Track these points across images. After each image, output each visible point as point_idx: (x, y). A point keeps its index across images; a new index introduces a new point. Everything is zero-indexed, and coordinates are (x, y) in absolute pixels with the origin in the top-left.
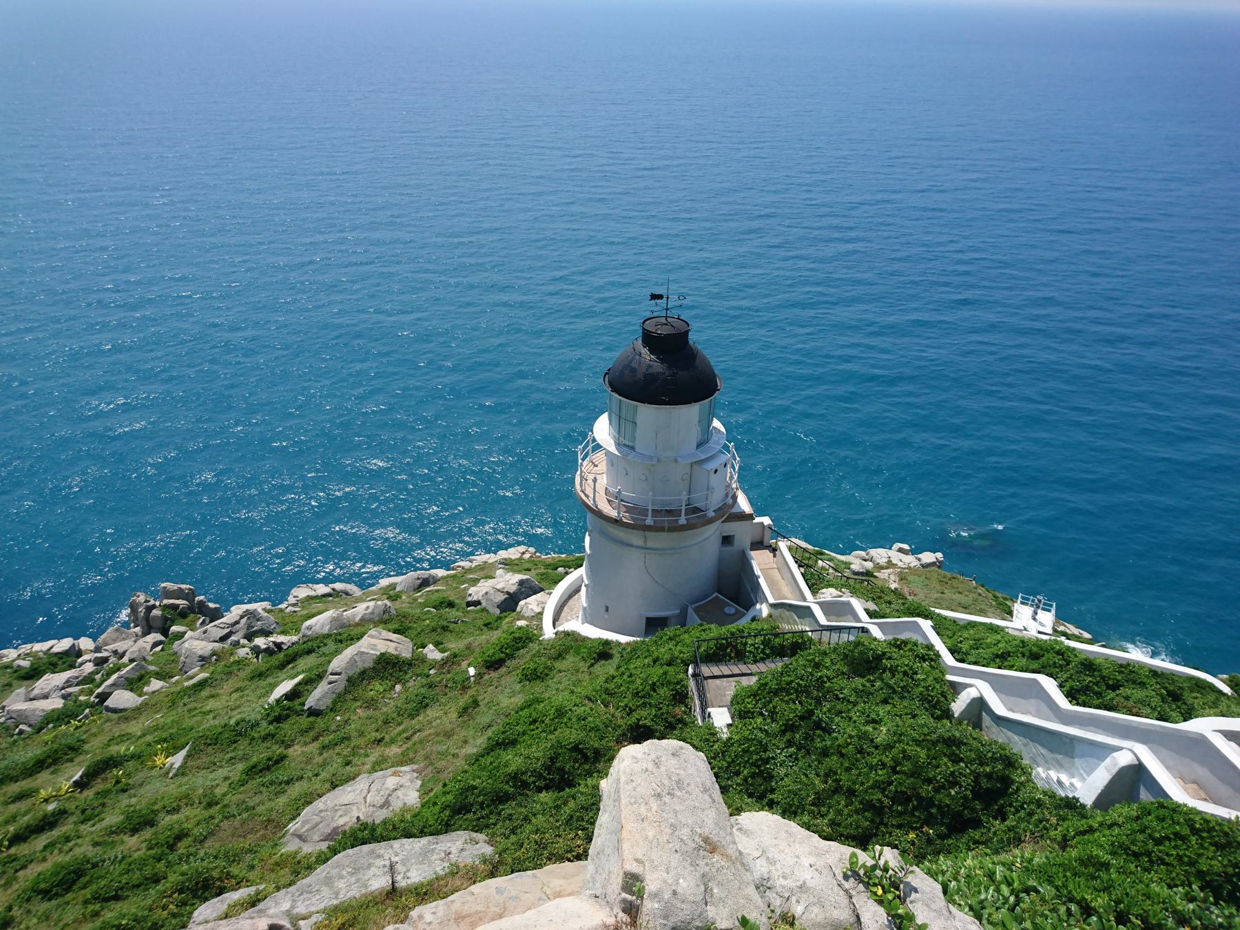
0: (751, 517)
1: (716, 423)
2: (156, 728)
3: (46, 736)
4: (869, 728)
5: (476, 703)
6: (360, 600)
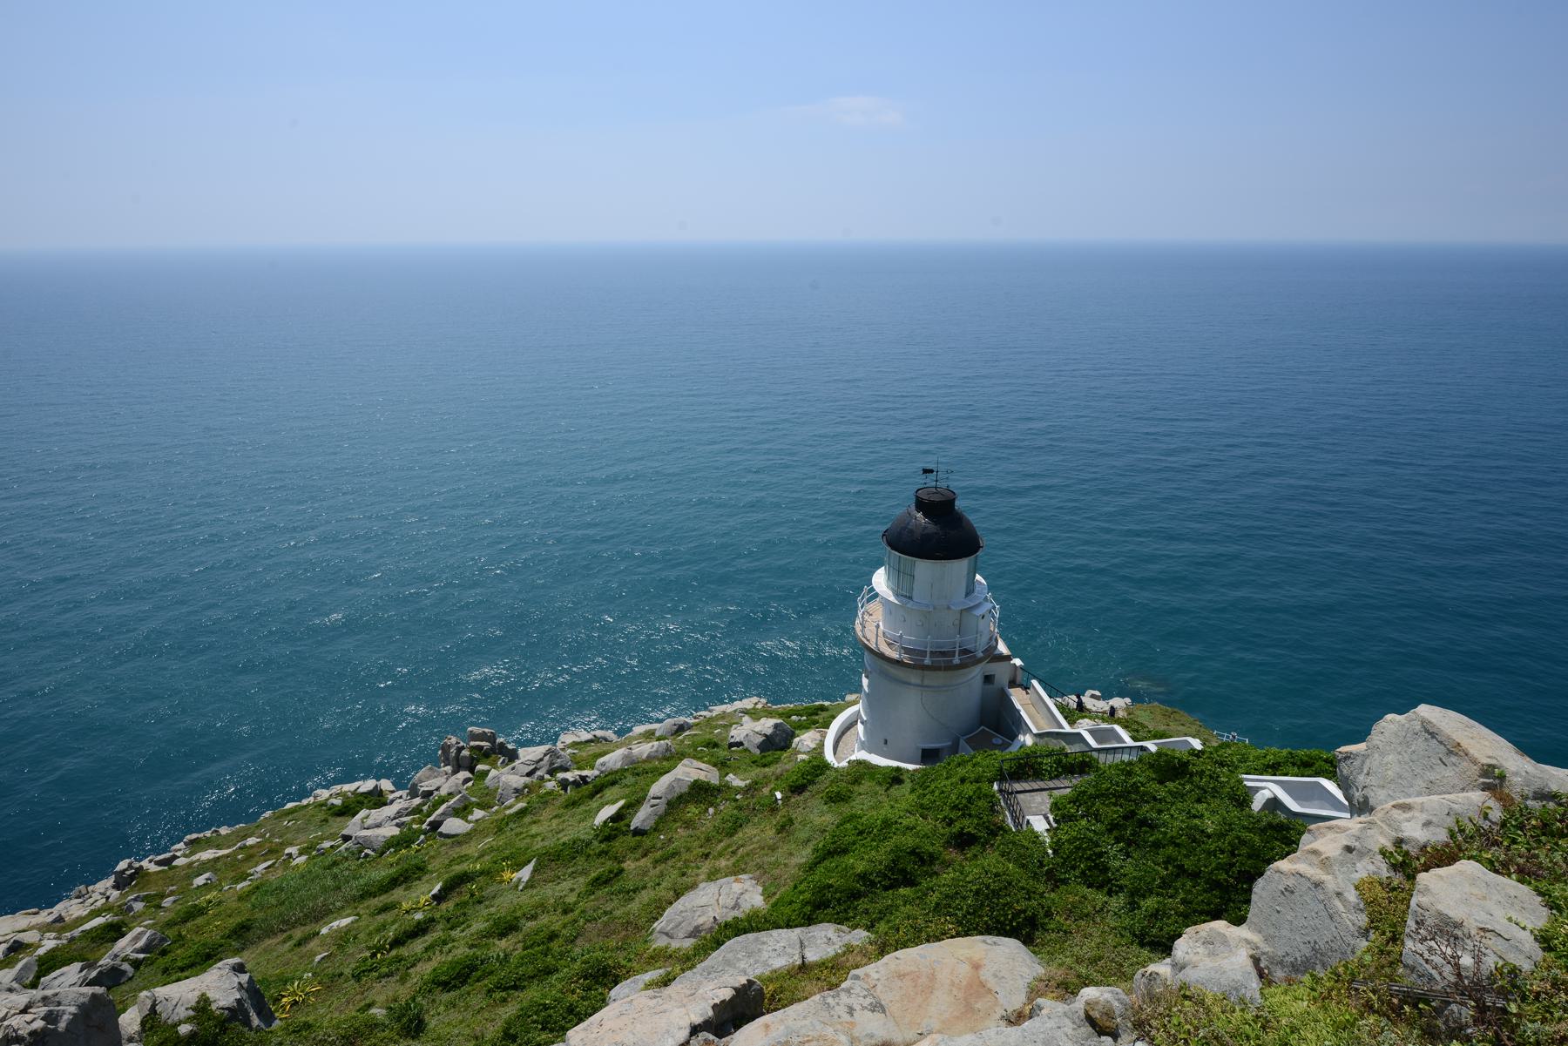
0: (1008, 658)
1: (978, 577)
2: (491, 849)
3: (390, 857)
4: (1196, 821)
5: (791, 821)
6: (618, 747)
